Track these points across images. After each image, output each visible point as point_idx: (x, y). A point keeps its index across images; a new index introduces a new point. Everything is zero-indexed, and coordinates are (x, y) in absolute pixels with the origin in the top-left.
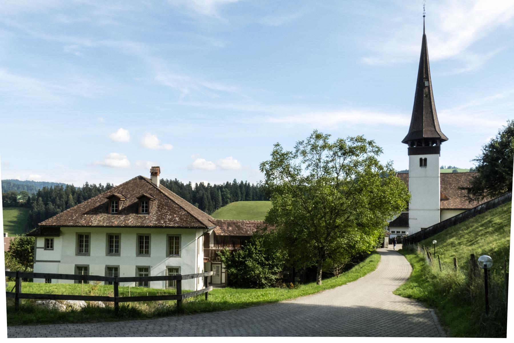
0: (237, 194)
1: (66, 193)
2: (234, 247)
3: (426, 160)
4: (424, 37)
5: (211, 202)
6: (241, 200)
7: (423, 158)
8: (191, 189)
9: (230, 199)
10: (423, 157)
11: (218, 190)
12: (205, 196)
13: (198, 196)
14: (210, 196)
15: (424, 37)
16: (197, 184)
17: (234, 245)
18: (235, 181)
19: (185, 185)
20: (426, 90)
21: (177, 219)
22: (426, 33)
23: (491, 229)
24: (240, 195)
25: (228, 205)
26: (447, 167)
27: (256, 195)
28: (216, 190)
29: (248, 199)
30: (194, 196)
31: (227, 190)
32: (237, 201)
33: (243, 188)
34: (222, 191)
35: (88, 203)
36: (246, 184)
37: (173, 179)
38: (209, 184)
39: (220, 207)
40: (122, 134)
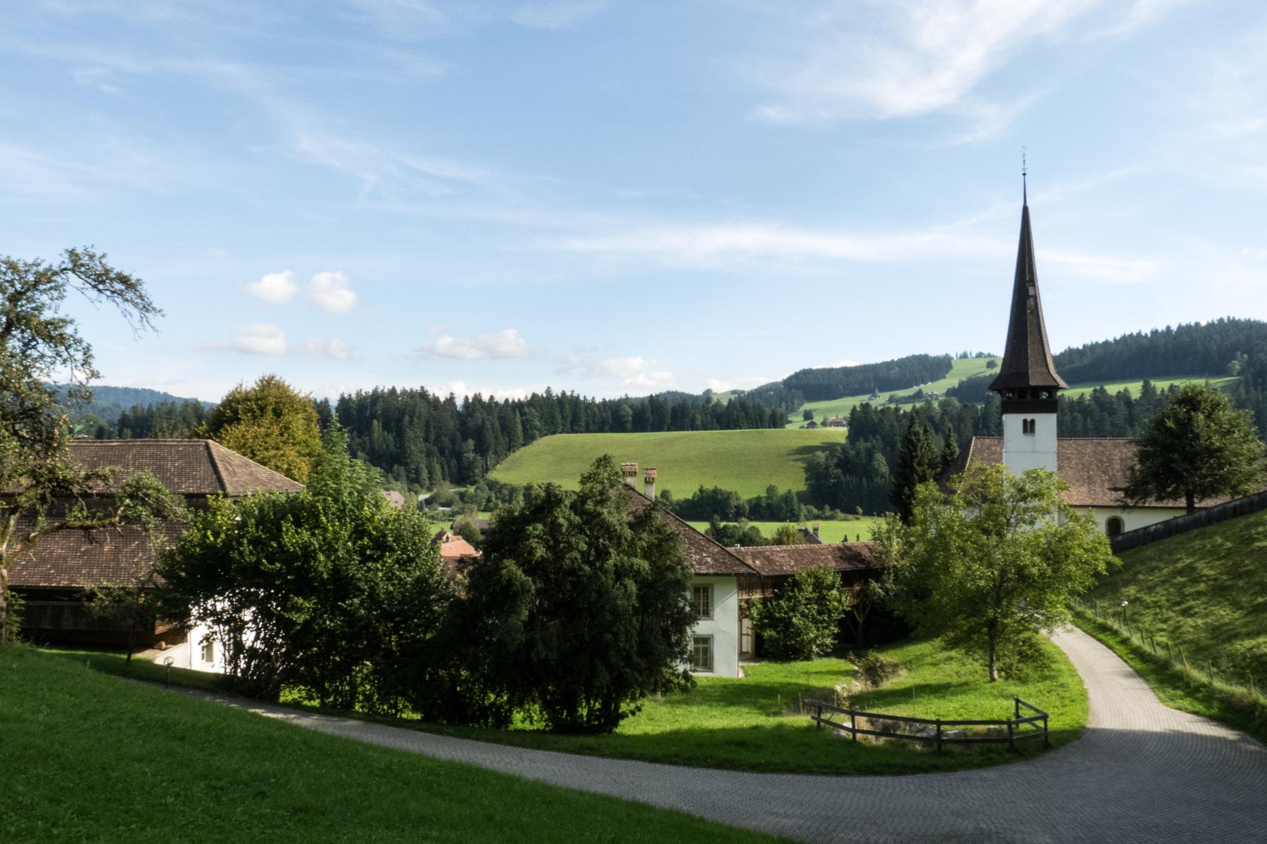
0: (553, 418)
1: (184, 420)
2: (763, 593)
3: (1033, 422)
8: (455, 406)
9: (539, 430)
10: (1029, 417)
13: (471, 424)
14: (497, 425)
16: (467, 398)
17: (763, 589)
18: (548, 391)
19: (442, 400)
20: (1031, 301)
21: (709, 560)
24: (559, 420)
25: (535, 443)
28: (509, 411)
30: (463, 424)
32: (554, 433)
34: (523, 414)
37: (417, 388)
38: (492, 397)
39: (518, 448)
40: (276, 285)
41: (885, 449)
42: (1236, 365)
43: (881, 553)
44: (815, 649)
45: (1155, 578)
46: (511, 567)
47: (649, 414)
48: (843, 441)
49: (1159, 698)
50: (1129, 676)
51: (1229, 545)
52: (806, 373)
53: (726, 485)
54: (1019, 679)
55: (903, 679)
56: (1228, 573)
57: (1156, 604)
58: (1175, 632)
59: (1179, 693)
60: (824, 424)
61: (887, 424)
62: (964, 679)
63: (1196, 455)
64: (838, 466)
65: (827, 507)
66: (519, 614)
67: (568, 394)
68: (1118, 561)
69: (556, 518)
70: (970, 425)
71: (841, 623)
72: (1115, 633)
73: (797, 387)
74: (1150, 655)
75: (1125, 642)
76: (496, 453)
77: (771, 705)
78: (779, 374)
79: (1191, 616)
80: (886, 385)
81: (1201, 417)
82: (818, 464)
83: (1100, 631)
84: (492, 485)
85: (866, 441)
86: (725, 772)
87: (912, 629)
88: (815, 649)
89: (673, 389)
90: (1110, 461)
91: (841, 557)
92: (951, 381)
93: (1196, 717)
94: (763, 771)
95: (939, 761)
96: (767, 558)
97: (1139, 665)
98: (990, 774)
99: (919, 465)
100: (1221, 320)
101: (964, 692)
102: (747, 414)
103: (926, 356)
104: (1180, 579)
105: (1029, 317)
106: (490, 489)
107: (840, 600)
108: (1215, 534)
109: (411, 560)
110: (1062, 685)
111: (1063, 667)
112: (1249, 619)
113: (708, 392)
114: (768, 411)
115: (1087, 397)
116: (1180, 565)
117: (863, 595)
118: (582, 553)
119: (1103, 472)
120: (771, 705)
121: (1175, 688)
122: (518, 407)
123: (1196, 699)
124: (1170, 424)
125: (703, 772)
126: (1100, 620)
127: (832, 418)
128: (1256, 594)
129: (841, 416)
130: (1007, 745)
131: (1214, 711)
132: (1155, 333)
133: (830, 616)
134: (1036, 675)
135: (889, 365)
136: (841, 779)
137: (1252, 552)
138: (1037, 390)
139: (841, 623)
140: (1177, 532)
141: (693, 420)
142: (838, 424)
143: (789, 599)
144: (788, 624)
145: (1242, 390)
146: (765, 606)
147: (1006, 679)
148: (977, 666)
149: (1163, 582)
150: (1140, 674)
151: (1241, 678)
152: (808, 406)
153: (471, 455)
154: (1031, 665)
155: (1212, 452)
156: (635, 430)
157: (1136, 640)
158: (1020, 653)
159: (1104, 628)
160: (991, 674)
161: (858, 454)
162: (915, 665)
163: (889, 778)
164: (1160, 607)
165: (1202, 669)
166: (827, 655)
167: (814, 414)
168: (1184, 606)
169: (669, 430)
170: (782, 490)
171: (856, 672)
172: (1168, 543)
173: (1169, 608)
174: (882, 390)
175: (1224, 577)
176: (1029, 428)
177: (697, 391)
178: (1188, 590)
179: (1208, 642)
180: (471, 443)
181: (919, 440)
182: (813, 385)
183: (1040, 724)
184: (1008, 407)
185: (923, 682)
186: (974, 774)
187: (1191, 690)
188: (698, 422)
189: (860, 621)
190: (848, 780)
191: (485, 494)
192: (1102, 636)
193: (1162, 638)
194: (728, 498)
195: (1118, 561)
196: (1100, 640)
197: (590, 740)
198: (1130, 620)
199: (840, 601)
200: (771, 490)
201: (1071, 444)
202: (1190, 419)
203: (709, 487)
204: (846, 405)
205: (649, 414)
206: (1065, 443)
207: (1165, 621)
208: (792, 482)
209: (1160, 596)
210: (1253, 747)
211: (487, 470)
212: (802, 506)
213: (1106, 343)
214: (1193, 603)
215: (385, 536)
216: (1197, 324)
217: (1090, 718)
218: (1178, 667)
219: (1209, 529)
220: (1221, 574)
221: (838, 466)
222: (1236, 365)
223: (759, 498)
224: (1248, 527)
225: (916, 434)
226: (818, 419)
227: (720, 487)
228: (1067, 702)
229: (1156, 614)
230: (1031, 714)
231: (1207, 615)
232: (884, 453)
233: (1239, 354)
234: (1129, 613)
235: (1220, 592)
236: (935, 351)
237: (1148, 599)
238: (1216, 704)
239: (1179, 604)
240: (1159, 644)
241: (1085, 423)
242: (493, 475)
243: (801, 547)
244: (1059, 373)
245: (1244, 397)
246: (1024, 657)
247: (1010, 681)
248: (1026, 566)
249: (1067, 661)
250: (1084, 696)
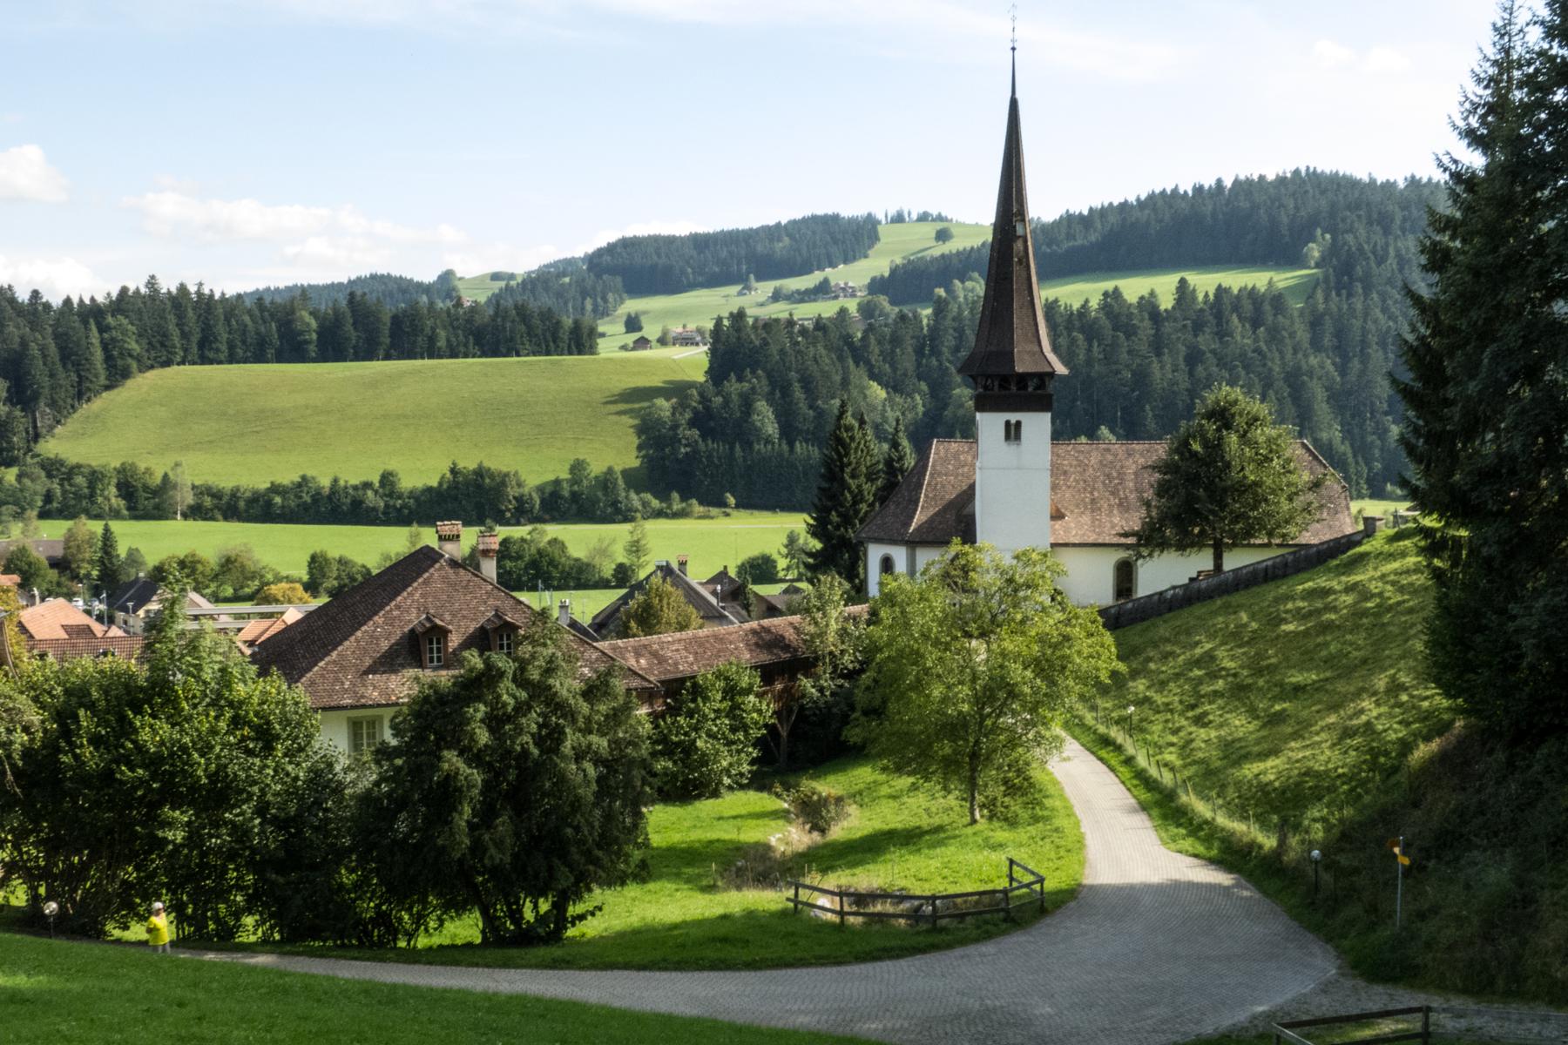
2: (651, 705)
3: (1018, 424)
4: (1014, 104)
5: (61, 373)
6: (183, 363)
7: (1013, 422)
9: (138, 359)
10: (1013, 417)
11: (85, 323)
12: (34, 350)
14: (53, 349)
15: (1014, 104)
18: (152, 283)
22: (1018, 96)
23: (1221, 682)
24: (176, 340)
25: (130, 383)
26: (914, 216)
27: (244, 342)
29: (211, 355)
31: (125, 321)
32: (167, 363)
33: (190, 313)
34: (102, 329)
35: (358, 641)
36: (199, 293)
39: (97, 393)
41: (772, 393)
42: (1314, 251)
43: (812, 636)
44: (727, 781)
45: (1168, 668)
46: (452, 760)
47: (349, 327)
48: (701, 378)
49: (1161, 839)
50: (1133, 811)
51: (1254, 625)
52: (628, 244)
53: (500, 460)
54: (1006, 819)
55: (852, 824)
56: (1249, 667)
57: (1168, 708)
58: (1186, 748)
59: (1183, 831)
60: (663, 341)
61: (774, 349)
62: (936, 821)
63: (1225, 490)
64: (692, 423)
65: (675, 496)
66: (461, 813)
67: (193, 289)
68: (1122, 667)
69: (499, 696)
70: (910, 349)
71: (758, 743)
72: (1119, 748)
73: (613, 271)
74: (1155, 781)
75: (1129, 761)
76: (53, 404)
77: (699, 876)
78: (582, 243)
79: (1205, 725)
80: (769, 267)
81: (1234, 438)
82: (659, 422)
83: (1102, 745)
84: (52, 467)
85: (740, 379)
86: (721, 974)
88: (727, 781)
89: (382, 270)
90: (1121, 476)
91: (757, 644)
92: (877, 264)
93: (1196, 861)
94: (760, 969)
95: (931, 939)
96: (655, 654)
97: (1146, 796)
98: (988, 948)
99: (853, 476)
100: (1297, 172)
101: (941, 843)
102: (530, 328)
103: (835, 218)
104: (1197, 672)
105: (1016, 268)
106: (50, 476)
107: (760, 709)
108: (1240, 607)
109: (301, 749)
110: (1057, 830)
111: (1058, 804)
112: (1264, 733)
113: (447, 276)
114: (568, 322)
115: (1094, 303)
116: (1198, 651)
117: (789, 699)
118: (533, 735)
119: (1112, 493)
120: (699, 876)
121: (1179, 825)
122: (92, 313)
123: (1198, 838)
124: (1196, 447)
125: (697, 975)
126: (1102, 729)
127: (676, 329)
128: (1275, 699)
129: (692, 326)
130: (1002, 915)
131: (1214, 853)
132: (1198, 190)
133: (747, 734)
134: (1025, 815)
135: (772, 233)
136: (842, 969)
137: (1278, 637)
138: (1023, 379)
139: (758, 743)
140: (1198, 599)
141: (432, 339)
142: (686, 341)
143: (690, 714)
144: (689, 749)
145: (1320, 295)
146: (657, 727)
147: (990, 819)
148: (952, 800)
149: (1177, 676)
150: (1144, 807)
151: (1241, 813)
152: (632, 305)
154: (1020, 800)
155: (1243, 488)
156: (323, 357)
157: (1142, 761)
158: (1006, 782)
159: (1106, 742)
160: (972, 814)
161: (727, 402)
162: (866, 799)
163: (889, 963)
164: (1171, 711)
165: (1208, 799)
166: (742, 787)
167: (644, 320)
168: (1199, 711)
169: (387, 357)
170: (596, 468)
171: (788, 812)
172: (1185, 617)
173: (1182, 714)
174: (761, 277)
175: (1245, 672)
176: (1013, 433)
178: (1206, 689)
179: (1218, 763)
181: (852, 438)
182: (642, 267)
183: (1037, 887)
184: (984, 404)
185: (886, 827)
186: (972, 950)
187: (1197, 829)
188: (442, 343)
189: (784, 734)
190: (849, 968)
191: (40, 485)
192: (1103, 753)
193: (1171, 756)
194: (503, 484)
195: (1122, 667)
196: (1101, 759)
197: (542, 952)
198: (1135, 728)
199: (760, 712)
200: (577, 467)
202: (1220, 438)
203: (468, 464)
204: (707, 306)
205: (349, 327)
206: (1062, 450)
207: (1175, 732)
208: (614, 452)
209: (1173, 695)
210: (1246, 893)
211: (36, 437)
212: (633, 495)
213: (1124, 206)
214: (1207, 707)
215: (268, 723)
216: (1262, 178)
217: (1087, 872)
218: (1184, 798)
219: (1236, 599)
220: (1242, 667)
221: (692, 423)
222: (1314, 251)
223: (557, 482)
224: (1277, 600)
225: (849, 428)
226: (651, 331)
227: (486, 464)
228: (1062, 853)
229: (1167, 721)
230: (1029, 878)
231: (1221, 726)
232: (771, 402)
233: (1319, 231)
234: (1135, 718)
235: (1239, 692)
236: (850, 209)
237: (1159, 699)
238: (1216, 844)
239: (1193, 707)
240: (1166, 765)
241: (1089, 350)
242: (50, 447)
243: (702, 633)
244: (1055, 349)
245: (1321, 307)
246: (1011, 789)
247: (996, 824)
248: (1016, 684)
249: (1063, 797)
250: (1080, 842)
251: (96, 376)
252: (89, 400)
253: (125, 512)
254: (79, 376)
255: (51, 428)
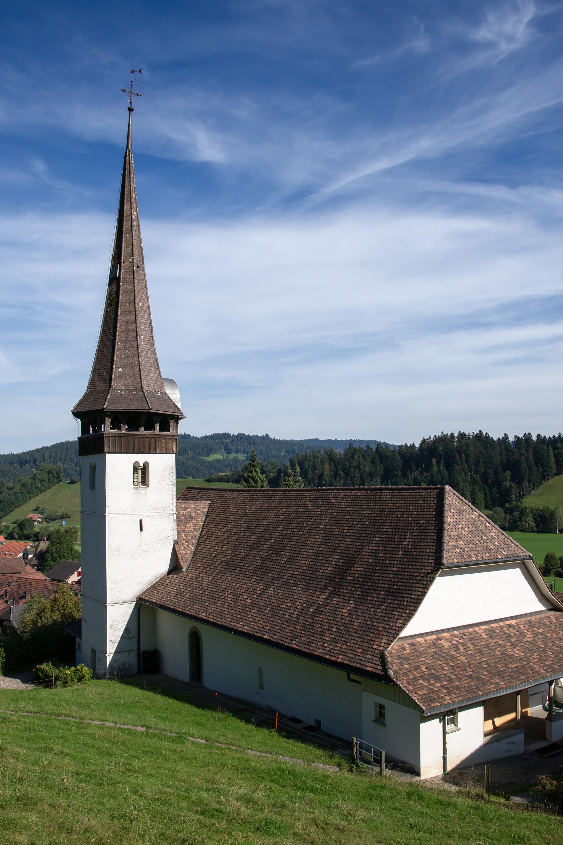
5: (534, 468)
10: (141, 458)
14: (531, 458)
34: (555, 449)
38: (539, 435)
87: (58, 668)
153: (508, 484)
176: (142, 474)
177: (261, 434)
180: (508, 474)
201: (183, 504)
211: (522, 496)
251: (552, 469)
252: (548, 479)
253: (536, 529)
254: (543, 469)
255: (530, 492)
